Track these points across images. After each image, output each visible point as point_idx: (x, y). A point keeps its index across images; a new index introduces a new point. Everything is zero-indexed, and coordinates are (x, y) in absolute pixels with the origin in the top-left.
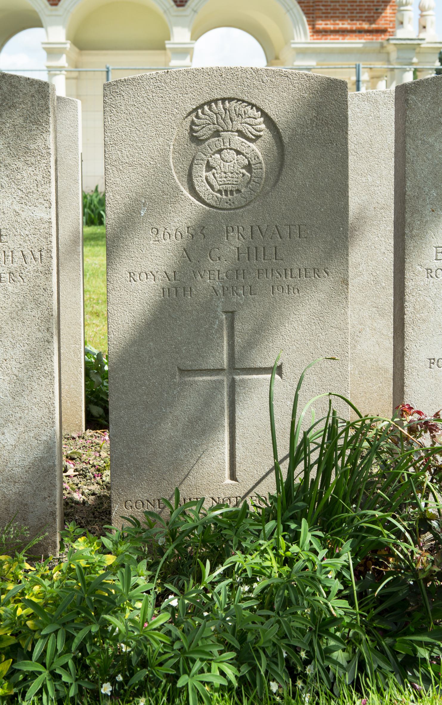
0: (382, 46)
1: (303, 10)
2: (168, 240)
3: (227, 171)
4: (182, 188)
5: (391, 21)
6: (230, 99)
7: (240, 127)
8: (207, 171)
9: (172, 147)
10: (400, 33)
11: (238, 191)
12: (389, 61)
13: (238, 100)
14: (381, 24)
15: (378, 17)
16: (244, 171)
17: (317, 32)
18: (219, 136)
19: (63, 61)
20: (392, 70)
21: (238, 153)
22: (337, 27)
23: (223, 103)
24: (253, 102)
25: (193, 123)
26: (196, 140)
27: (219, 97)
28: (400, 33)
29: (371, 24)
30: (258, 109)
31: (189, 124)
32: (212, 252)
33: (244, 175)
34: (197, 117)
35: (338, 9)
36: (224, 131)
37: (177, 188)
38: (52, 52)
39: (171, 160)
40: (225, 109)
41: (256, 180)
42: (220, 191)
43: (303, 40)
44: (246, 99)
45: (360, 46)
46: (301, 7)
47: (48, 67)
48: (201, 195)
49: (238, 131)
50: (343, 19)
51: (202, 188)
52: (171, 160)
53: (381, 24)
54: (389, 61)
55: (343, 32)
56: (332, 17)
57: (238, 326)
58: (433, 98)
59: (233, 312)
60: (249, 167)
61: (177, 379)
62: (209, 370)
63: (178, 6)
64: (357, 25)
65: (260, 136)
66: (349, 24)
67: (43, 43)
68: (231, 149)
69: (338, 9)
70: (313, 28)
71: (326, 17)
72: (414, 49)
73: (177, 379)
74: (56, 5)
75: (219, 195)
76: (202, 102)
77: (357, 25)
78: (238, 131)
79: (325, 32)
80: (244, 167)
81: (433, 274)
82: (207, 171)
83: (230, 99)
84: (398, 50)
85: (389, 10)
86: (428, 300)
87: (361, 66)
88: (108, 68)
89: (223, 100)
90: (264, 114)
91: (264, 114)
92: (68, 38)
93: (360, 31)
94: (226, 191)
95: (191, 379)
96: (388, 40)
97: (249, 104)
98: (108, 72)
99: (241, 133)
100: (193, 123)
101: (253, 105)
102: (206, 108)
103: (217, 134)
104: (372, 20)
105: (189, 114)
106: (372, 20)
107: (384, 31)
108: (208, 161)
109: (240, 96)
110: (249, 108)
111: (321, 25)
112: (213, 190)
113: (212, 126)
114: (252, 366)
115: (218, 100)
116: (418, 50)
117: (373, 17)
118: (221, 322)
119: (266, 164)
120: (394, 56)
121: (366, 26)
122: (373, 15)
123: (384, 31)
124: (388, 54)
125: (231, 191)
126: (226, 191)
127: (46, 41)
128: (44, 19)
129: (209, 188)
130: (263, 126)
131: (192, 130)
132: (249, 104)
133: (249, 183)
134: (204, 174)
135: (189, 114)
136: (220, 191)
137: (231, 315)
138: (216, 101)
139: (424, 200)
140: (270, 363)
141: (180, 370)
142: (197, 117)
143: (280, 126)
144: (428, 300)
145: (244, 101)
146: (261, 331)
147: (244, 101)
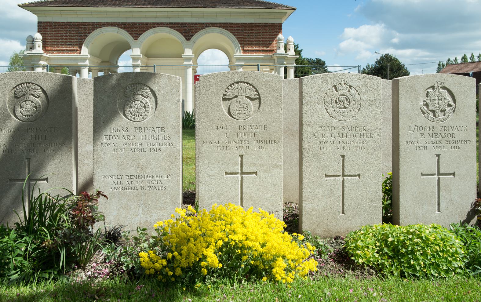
0: (272, 57)
1: (239, 42)
2: (6, 133)
3: (28, 108)
4: (11, 114)
5: (275, 47)
6: (29, 83)
7: (32, 93)
8: (20, 108)
9: (7, 100)
10: (279, 52)
11: (32, 115)
12: (274, 63)
13: (32, 83)
14: (271, 48)
15: (270, 45)
16: (34, 108)
17: (245, 51)
18: (25, 96)
19: (139, 63)
20: (276, 66)
21: (32, 102)
22: (253, 49)
23: (26, 84)
24: (37, 84)
25: (15, 91)
26: (16, 97)
27: (25, 82)
28: (279, 52)
29: (267, 48)
30: (39, 86)
31: (14, 92)
32: (22, 137)
33: (34, 110)
34: (17, 89)
35: (254, 42)
36: (27, 94)
37: (9, 114)
38: (135, 59)
39: (7, 105)
40: (27, 86)
41: (38, 111)
42: (25, 115)
43: (239, 54)
44: (35, 83)
45: (263, 56)
46: (238, 41)
47: (133, 65)
48: (18, 117)
49: (32, 94)
50: (255, 45)
51: (19, 114)
52: (7, 105)
53: (271, 48)
54: (274, 63)
55: (256, 51)
56: (251, 45)
57: (31, 164)
58: (103, 83)
59: (30, 159)
60: (36, 107)
61: (8, 183)
62: (21, 180)
63: (187, 40)
64: (261, 48)
65: (40, 96)
66: (258, 48)
67: (131, 55)
68: (29, 100)
69: (254, 42)
70: (243, 49)
71: (249, 45)
72: (284, 58)
73: (8, 183)
74: (137, 40)
75: (25, 117)
76: (18, 84)
77: (261, 48)
78: (32, 94)
79: (248, 51)
80: (34, 107)
81: (104, 145)
82: (20, 108)
83: (29, 83)
84: (278, 58)
85: (274, 42)
86: (102, 154)
87: (260, 65)
88: (154, 66)
89: (26, 83)
90: (41, 88)
91: (41, 88)
92: (141, 53)
93: (263, 51)
94: (27, 115)
95: (14, 183)
96: (274, 54)
97: (36, 85)
98: (154, 67)
99: (33, 95)
100: (15, 91)
101: (37, 85)
102: (23, 85)
103: (24, 95)
104: (268, 46)
105: (14, 88)
106: (268, 46)
107: (273, 51)
108: (21, 105)
109: (33, 82)
110: (36, 86)
111: (246, 48)
112: (22, 115)
113: (22, 92)
114: (37, 178)
115: (25, 83)
116: (286, 58)
117: (268, 45)
118: (25, 162)
119: (42, 106)
120: (276, 61)
121: (265, 49)
122: (268, 44)
123: (273, 51)
124: (274, 60)
125: (29, 115)
126: (27, 115)
127: (132, 54)
128: (132, 45)
129: (21, 114)
130: (41, 92)
131: (15, 94)
132: (36, 85)
133: (36, 112)
134: (19, 109)
135: (14, 88)
136: (25, 115)
137: (29, 160)
138: (24, 83)
139: (100, 119)
140: (45, 177)
141: (10, 179)
142: (17, 89)
143: (47, 92)
144: (102, 154)
145: (34, 84)
146: (40, 166)
147: (34, 84)
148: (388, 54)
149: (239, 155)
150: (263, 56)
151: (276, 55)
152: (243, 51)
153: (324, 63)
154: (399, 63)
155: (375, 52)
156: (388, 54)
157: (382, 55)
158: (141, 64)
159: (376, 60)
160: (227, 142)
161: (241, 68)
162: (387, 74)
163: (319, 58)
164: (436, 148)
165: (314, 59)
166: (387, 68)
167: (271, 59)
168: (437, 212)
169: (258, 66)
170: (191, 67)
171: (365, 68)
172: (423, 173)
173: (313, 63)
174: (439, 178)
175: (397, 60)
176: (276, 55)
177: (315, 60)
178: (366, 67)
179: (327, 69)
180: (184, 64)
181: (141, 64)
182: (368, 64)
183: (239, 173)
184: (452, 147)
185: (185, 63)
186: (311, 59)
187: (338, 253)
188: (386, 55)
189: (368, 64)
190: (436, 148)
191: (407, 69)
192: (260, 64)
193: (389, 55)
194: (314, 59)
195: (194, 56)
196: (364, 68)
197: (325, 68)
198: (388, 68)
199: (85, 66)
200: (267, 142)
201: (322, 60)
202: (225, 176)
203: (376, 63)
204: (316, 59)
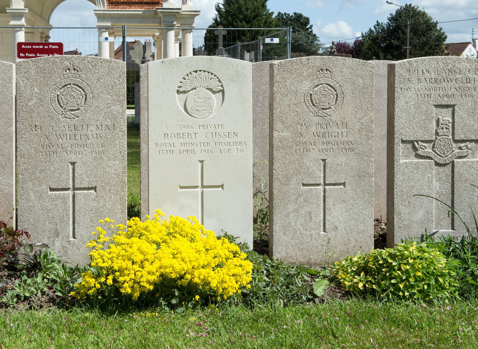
43: (102, 9)
45: (141, 13)
47: (97, 26)
84: (164, 16)
87: (126, 27)
124: (160, 18)
148: (410, 5)
149: (199, 161)
150: (141, 13)
151: (160, 11)
152: (109, 3)
153: (307, 20)
154: (429, 19)
155: (387, 2)
156: (410, 5)
157: (399, 8)
158: (25, 24)
159: (390, 16)
160: (183, 144)
161: (105, 32)
162: (406, 39)
163: (299, 11)
164: (182, 152)
165: (291, 15)
166: (406, 28)
167: (155, 18)
168: (322, 233)
169: (124, 28)
170: (23, 29)
171: (373, 29)
172: (181, 185)
173: (290, 20)
174: (203, 191)
175: (424, 14)
176: (160, 11)
177: (292, 16)
178: (375, 27)
179: (312, 31)
180: (10, 24)
181: (25, 24)
182: (377, 22)
183: (199, 186)
184: (203, 151)
185: (13, 23)
186: (285, 14)
187: (48, 283)
188: (406, 6)
189: (377, 22)
190: (182, 152)
191: (441, 29)
192: (126, 25)
193: (412, 6)
194: (291, 15)
195: (27, 11)
196: (370, 29)
197: (308, 29)
198: (408, 28)
199: (20, 27)
200: (231, 145)
201: (305, 15)
202: (50, 193)
203: (390, 21)
204: (295, 13)
